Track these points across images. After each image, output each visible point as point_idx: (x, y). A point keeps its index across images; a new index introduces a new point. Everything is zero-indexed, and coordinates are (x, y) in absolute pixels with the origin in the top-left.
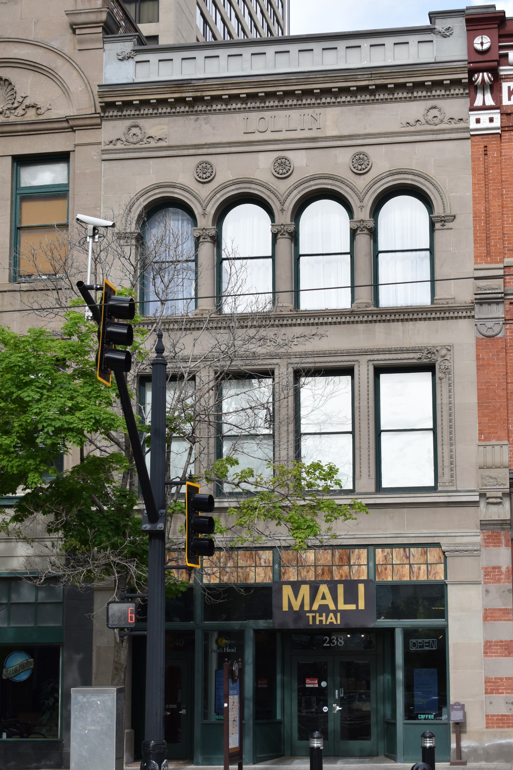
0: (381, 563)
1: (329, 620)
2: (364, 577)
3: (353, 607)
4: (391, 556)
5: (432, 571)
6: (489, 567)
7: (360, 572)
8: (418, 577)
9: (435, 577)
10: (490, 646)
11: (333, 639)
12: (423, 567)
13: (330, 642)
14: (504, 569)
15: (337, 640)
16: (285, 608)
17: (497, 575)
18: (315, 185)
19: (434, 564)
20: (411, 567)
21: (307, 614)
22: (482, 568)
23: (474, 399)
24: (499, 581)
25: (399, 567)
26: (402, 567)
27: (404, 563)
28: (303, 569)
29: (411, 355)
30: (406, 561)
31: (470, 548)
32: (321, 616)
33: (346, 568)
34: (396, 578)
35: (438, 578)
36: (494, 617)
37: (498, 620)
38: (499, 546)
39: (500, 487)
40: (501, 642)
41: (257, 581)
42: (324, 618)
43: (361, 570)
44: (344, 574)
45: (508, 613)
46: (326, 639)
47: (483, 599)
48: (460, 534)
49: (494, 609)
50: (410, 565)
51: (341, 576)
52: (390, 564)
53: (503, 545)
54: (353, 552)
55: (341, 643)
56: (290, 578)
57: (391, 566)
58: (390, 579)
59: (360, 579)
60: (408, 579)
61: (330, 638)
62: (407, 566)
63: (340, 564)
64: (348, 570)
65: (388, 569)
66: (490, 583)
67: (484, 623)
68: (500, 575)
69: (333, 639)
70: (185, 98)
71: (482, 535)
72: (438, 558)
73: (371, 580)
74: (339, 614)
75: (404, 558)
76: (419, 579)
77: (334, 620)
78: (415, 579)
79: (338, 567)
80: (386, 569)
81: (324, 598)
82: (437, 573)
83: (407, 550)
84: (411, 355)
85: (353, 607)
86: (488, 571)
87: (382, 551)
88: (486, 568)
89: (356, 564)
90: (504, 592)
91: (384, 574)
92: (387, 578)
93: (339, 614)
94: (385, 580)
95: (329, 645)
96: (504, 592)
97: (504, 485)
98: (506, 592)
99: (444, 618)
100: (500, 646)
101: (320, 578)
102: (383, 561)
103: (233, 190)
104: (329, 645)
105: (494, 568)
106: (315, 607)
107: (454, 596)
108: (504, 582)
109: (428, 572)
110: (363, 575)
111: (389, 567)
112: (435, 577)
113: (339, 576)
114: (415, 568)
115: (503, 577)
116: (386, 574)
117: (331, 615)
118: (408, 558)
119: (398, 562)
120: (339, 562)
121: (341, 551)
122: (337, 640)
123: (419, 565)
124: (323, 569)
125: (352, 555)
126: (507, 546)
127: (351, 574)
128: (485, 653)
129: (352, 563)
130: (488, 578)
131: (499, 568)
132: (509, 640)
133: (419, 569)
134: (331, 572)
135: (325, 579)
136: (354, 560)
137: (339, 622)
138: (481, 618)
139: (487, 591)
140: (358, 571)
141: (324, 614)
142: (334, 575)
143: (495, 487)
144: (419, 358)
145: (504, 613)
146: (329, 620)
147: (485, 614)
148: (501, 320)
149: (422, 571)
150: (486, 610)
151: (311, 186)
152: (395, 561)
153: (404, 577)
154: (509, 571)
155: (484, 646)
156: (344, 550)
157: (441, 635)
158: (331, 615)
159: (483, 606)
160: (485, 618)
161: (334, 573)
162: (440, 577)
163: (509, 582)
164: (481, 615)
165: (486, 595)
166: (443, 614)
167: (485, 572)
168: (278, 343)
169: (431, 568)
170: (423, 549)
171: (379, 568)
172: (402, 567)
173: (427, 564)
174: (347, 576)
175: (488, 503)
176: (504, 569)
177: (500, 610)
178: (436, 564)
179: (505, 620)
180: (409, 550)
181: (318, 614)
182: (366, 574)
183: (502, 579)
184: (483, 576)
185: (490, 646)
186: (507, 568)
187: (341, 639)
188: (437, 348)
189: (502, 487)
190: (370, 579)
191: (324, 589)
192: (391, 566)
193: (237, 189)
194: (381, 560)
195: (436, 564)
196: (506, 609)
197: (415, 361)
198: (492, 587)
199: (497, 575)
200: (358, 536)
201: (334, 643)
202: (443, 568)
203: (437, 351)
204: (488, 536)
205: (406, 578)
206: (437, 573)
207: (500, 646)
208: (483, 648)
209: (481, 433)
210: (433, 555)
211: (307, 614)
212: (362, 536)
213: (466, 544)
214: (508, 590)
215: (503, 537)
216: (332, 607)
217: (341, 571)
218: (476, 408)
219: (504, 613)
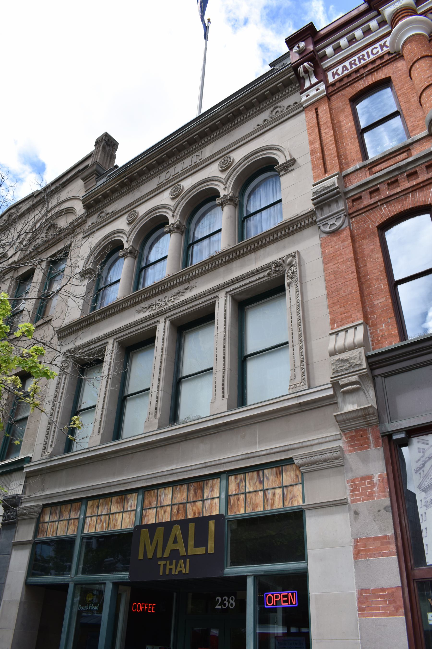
0: (234, 493)
1: (178, 569)
2: (216, 513)
3: (201, 551)
4: (244, 483)
5: (289, 495)
6: (357, 478)
7: (212, 506)
8: (272, 505)
9: (292, 503)
10: (366, 598)
11: (225, 600)
12: (279, 492)
13: (223, 603)
14: (376, 479)
15: (229, 602)
16: (141, 557)
17: (368, 488)
18: (196, 191)
19: (290, 486)
20: (264, 494)
21: (159, 563)
22: (348, 482)
23: (323, 291)
24: (370, 496)
25: (252, 495)
26: (255, 495)
27: (258, 489)
28: (161, 510)
29: (261, 275)
30: (259, 487)
31: (328, 456)
32: (171, 564)
33: (199, 504)
34: (249, 510)
35: (295, 504)
36: (369, 550)
37: (374, 555)
38: (367, 448)
39: (355, 370)
40: (383, 590)
41: (50, 508)
42: (173, 567)
43: (214, 505)
44: (197, 512)
45: (389, 543)
46: (218, 599)
47: (351, 524)
48: (316, 442)
49: (368, 539)
50: (264, 491)
51: (195, 514)
52: (243, 493)
53: (372, 445)
54: (207, 484)
55: (232, 605)
56: (149, 520)
57: (243, 496)
58: (242, 511)
59: (212, 514)
60: (262, 509)
61: (222, 598)
62: (261, 493)
63: (194, 500)
64: (201, 506)
65: (241, 499)
66: (359, 500)
67: (355, 562)
68: (372, 488)
69: (225, 600)
70: (124, 181)
71: (344, 438)
72: (295, 477)
73: (222, 515)
74: (188, 560)
75: (257, 483)
76: (274, 508)
77: (183, 569)
78: (269, 508)
79: (192, 504)
80: (238, 500)
81: (175, 541)
82: (295, 497)
83: (261, 472)
84: (261, 275)
85: (201, 551)
86: (355, 485)
87: (235, 478)
88: (353, 481)
89: (209, 497)
90: (379, 511)
91: (236, 505)
92: (239, 511)
93: (188, 560)
94: (238, 513)
95: (220, 607)
96: (379, 511)
97: (359, 365)
98: (383, 511)
99: (305, 560)
100: (381, 597)
101: (175, 519)
102: (236, 490)
103: (146, 219)
104: (220, 607)
105: (363, 479)
106: (166, 555)
107: (315, 528)
108: (379, 497)
109: (284, 497)
110: (216, 510)
111: (242, 497)
112: (292, 503)
113: (192, 514)
114: (269, 493)
115: (376, 489)
116: (238, 505)
117: (181, 562)
118: (262, 482)
119: (251, 490)
120: (193, 497)
121: (196, 484)
122: (229, 602)
123: (273, 490)
124: (178, 508)
125: (205, 487)
126: (376, 445)
127: (204, 509)
128: (360, 609)
129: (205, 498)
130: (356, 494)
131: (370, 477)
132: (394, 586)
133: (274, 494)
134: (185, 510)
135: (180, 519)
136: (207, 493)
137: (187, 572)
138: (351, 555)
139: (356, 513)
140: (211, 506)
141: (174, 562)
142: (188, 514)
143: (348, 371)
144: (269, 274)
145: (382, 544)
146: (178, 569)
147: (356, 547)
148: (342, 213)
149: (277, 496)
150: (357, 541)
151: (193, 193)
152: (248, 489)
153: (257, 507)
154: (383, 480)
155: (358, 599)
156: (199, 483)
157: (299, 582)
158: (181, 562)
159: (352, 535)
160: (357, 554)
161: (188, 511)
162: (298, 502)
163: (385, 496)
164: (351, 550)
165: (356, 519)
166: (301, 555)
167: (352, 486)
168: (160, 305)
169: (287, 492)
170: (277, 469)
171: (232, 499)
172: (255, 495)
173: (283, 487)
174: (199, 513)
175: (345, 393)
176: (376, 479)
177: (375, 539)
178: (293, 485)
179: (384, 555)
180: (263, 473)
181: (168, 562)
182: (218, 508)
183: (374, 493)
184: (349, 492)
185: (366, 598)
186: (380, 476)
187: (232, 599)
188: (283, 259)
189: (357, 369)
190: (221, 513)
191: (177, 531)
192: (243, 496)
193: (148, 218)
194: (234, 489)
195: (293, 485)
196: (385, 537)
197: (266, 278)
198: (363, 506)
199: (368, 488)
200: (210, 464)
201: (225, 605)
202: (301, 490)
203: (284, 261)
204: (351, 437)
205: (260, 509)
206: (295, 497)
207: (381, 597)
208: (356, 602)
209: (333, 322)
210: (289, 476)
211: (159, 563)
212: (213, 463)
213: (322, 452)
214: (385, 508)
215: (370, 435)
216: (183, 552)
217: (194, 508)
218: (325, 297)
219: (382, 544)
